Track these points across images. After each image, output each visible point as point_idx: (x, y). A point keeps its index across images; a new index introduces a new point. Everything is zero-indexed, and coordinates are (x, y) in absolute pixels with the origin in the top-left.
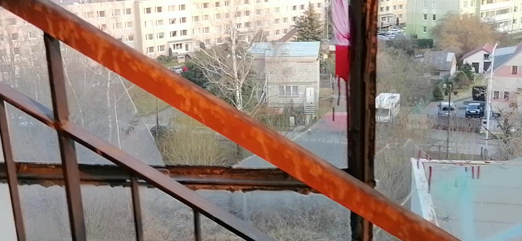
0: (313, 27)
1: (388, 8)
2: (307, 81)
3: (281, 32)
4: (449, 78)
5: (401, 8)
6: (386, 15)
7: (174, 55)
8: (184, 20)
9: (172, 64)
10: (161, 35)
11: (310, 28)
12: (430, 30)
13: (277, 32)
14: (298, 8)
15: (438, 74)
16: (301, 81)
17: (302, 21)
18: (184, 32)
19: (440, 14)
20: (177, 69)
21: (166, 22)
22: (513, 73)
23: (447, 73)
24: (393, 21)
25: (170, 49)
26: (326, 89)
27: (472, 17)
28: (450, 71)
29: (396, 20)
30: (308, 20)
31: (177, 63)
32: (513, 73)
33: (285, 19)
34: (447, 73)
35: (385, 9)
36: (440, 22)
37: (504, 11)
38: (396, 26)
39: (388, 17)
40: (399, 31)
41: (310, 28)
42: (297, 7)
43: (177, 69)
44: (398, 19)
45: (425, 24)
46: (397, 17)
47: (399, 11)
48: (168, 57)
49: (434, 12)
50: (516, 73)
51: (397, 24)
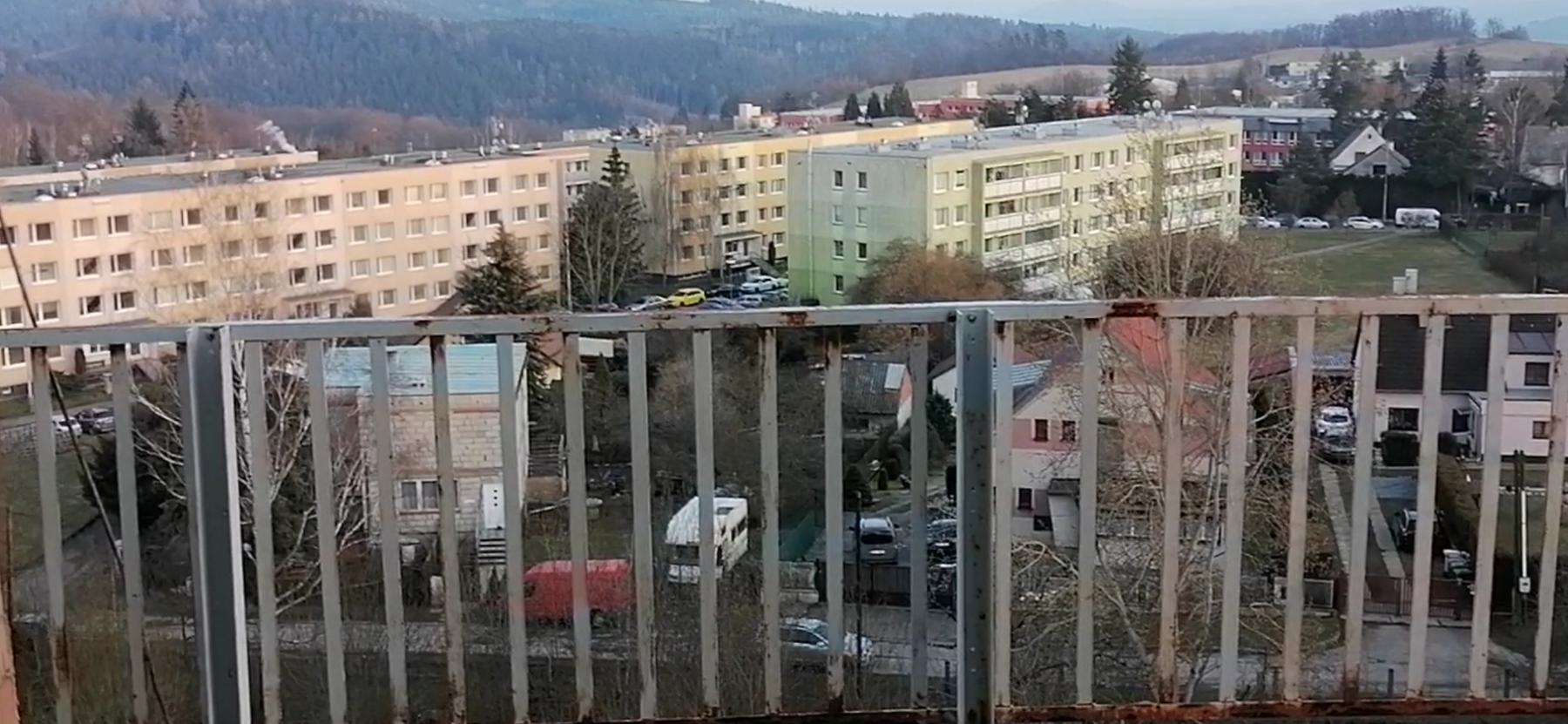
0: (511, 293)
1: (742, 216)
2: (484, 465)
3: (430, 291)
4: (892, 438)
5: (779, 215)
6: (738, 234)
7: (91, 370)
8: (124, 260)
9: (85, 398)
10: (49, 310)
11: (501, 295)
12: (850, 289)
13: (419, 291)
14: (480, 219)
15: (865, 424)
16: (466, 466)
17: (479, 275)
18: (127, 299)
19: (877, 242)
20: (98, 415)
21: (68, 268)
22: (1037, 439)
23: (885, 422)
24: (759, 250)
25: (80, 352)
26: (547, 479)
27: (959, 253)
28: (895, 415)
29: (766, 248)
30: (496, 272)
31: (100, 395)
32: (1037, 439)
33: (442, 254)
34: (885, 422)
35: (733, 219)
36: (877, 268)
37: (1044, 233)
38: (766, 267)
39: (746, 242)
40: (775, 281)
41: (501, 295)
42: (475, 218)
43: (98, 415)
44: (771, 245)
45: (838, 268)
46: (769, 239)
47: (776, 223)
48: (72, 377)
49: (861, 236)
50: (1046, 439)
51: (771, 261)
